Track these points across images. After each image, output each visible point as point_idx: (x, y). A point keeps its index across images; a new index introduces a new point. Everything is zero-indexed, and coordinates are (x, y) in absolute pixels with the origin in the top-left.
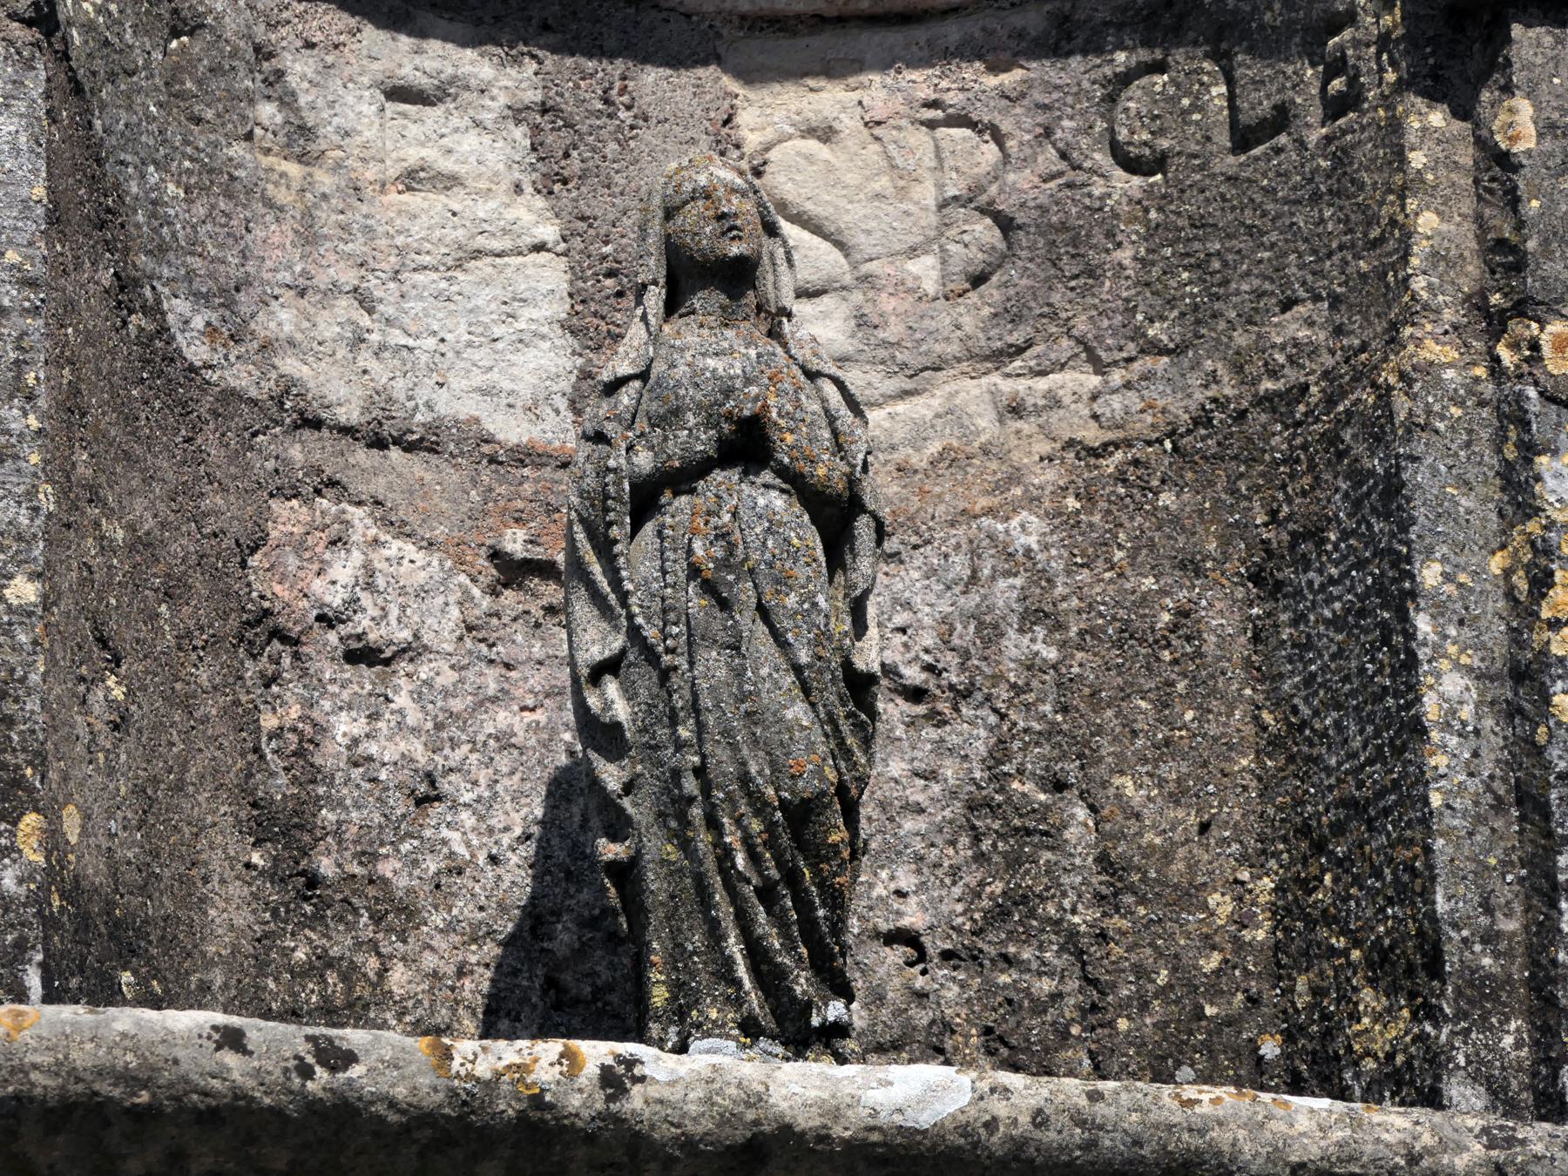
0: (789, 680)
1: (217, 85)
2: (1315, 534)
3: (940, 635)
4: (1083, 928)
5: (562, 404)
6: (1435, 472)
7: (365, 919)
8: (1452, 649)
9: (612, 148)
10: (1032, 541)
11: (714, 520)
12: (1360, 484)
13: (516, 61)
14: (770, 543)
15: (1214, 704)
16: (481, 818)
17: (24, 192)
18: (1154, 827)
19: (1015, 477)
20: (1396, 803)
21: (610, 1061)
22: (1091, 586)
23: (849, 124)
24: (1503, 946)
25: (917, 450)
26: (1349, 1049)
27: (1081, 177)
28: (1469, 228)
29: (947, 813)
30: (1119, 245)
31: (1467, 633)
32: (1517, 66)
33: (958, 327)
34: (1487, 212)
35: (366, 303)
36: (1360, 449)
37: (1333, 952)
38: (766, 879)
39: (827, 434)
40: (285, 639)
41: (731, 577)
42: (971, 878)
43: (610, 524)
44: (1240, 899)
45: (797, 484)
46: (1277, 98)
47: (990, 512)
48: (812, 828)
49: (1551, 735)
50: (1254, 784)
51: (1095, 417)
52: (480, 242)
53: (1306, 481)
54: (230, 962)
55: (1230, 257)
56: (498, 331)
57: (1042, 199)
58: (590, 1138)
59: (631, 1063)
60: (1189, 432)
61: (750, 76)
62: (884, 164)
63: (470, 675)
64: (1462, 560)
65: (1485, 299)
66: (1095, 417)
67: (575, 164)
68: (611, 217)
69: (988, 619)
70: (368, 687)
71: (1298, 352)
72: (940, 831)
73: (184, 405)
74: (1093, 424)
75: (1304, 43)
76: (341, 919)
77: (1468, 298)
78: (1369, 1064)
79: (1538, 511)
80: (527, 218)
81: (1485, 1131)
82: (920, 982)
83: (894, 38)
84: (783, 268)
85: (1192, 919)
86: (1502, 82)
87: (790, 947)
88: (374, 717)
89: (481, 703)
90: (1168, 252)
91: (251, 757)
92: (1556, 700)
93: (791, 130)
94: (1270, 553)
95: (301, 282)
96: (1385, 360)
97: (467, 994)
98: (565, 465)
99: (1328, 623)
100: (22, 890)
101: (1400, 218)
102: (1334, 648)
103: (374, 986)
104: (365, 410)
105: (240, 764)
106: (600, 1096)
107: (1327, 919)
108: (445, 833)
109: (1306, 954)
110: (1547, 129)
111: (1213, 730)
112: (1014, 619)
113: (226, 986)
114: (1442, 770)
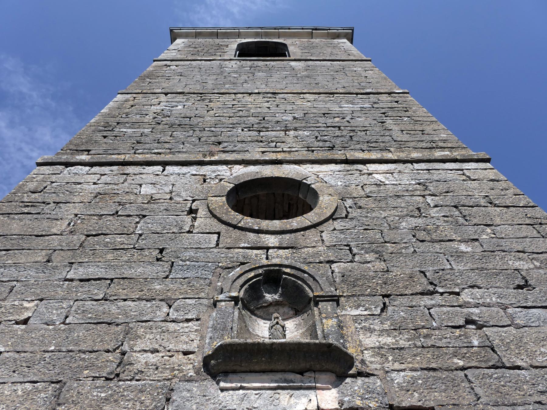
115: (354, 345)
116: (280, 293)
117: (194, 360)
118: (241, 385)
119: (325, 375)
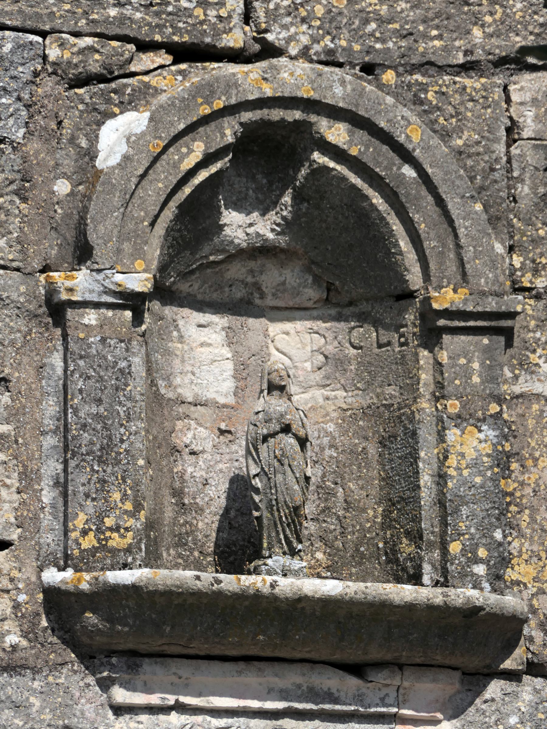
0: (295, 480)
1: (167, 331)
2: (395, 437)
5: (232, 394)
6: (424, 431)
9: (243, 336)
10: (332, 430)
13: (223, 317)
19: (327, 414)
23: (292, 332)
27: (343, 349)
28: (432, 377)
31: (430, 466)
35: (193, 374)
37: (396, 528)
39: (300, 423)
42: (317, 502)
45: (296, 437)
47: (322, 422)
52: (216, 358)
53: (393, 425)
54: (168, 525)
56: (219, 378)
58: (267, 598)
61: (272, 320)
63: (214, 457)
67: (235, 340)
71: (392, 397)
78: (404, 554)
79: (445, 442)
80: (225, 352)
81: (442, 593)
83: (302, 313)
84: (291, 385)
87: (292, 535)
88: (196, 467)
94: (383, 438)
108: (209, 492)
111: (370, 475)
112: (327, 447)
115: (535, 548)
116: (284, 218)
117: (12, 580)
118: (177, 701)
119: (434, 681)
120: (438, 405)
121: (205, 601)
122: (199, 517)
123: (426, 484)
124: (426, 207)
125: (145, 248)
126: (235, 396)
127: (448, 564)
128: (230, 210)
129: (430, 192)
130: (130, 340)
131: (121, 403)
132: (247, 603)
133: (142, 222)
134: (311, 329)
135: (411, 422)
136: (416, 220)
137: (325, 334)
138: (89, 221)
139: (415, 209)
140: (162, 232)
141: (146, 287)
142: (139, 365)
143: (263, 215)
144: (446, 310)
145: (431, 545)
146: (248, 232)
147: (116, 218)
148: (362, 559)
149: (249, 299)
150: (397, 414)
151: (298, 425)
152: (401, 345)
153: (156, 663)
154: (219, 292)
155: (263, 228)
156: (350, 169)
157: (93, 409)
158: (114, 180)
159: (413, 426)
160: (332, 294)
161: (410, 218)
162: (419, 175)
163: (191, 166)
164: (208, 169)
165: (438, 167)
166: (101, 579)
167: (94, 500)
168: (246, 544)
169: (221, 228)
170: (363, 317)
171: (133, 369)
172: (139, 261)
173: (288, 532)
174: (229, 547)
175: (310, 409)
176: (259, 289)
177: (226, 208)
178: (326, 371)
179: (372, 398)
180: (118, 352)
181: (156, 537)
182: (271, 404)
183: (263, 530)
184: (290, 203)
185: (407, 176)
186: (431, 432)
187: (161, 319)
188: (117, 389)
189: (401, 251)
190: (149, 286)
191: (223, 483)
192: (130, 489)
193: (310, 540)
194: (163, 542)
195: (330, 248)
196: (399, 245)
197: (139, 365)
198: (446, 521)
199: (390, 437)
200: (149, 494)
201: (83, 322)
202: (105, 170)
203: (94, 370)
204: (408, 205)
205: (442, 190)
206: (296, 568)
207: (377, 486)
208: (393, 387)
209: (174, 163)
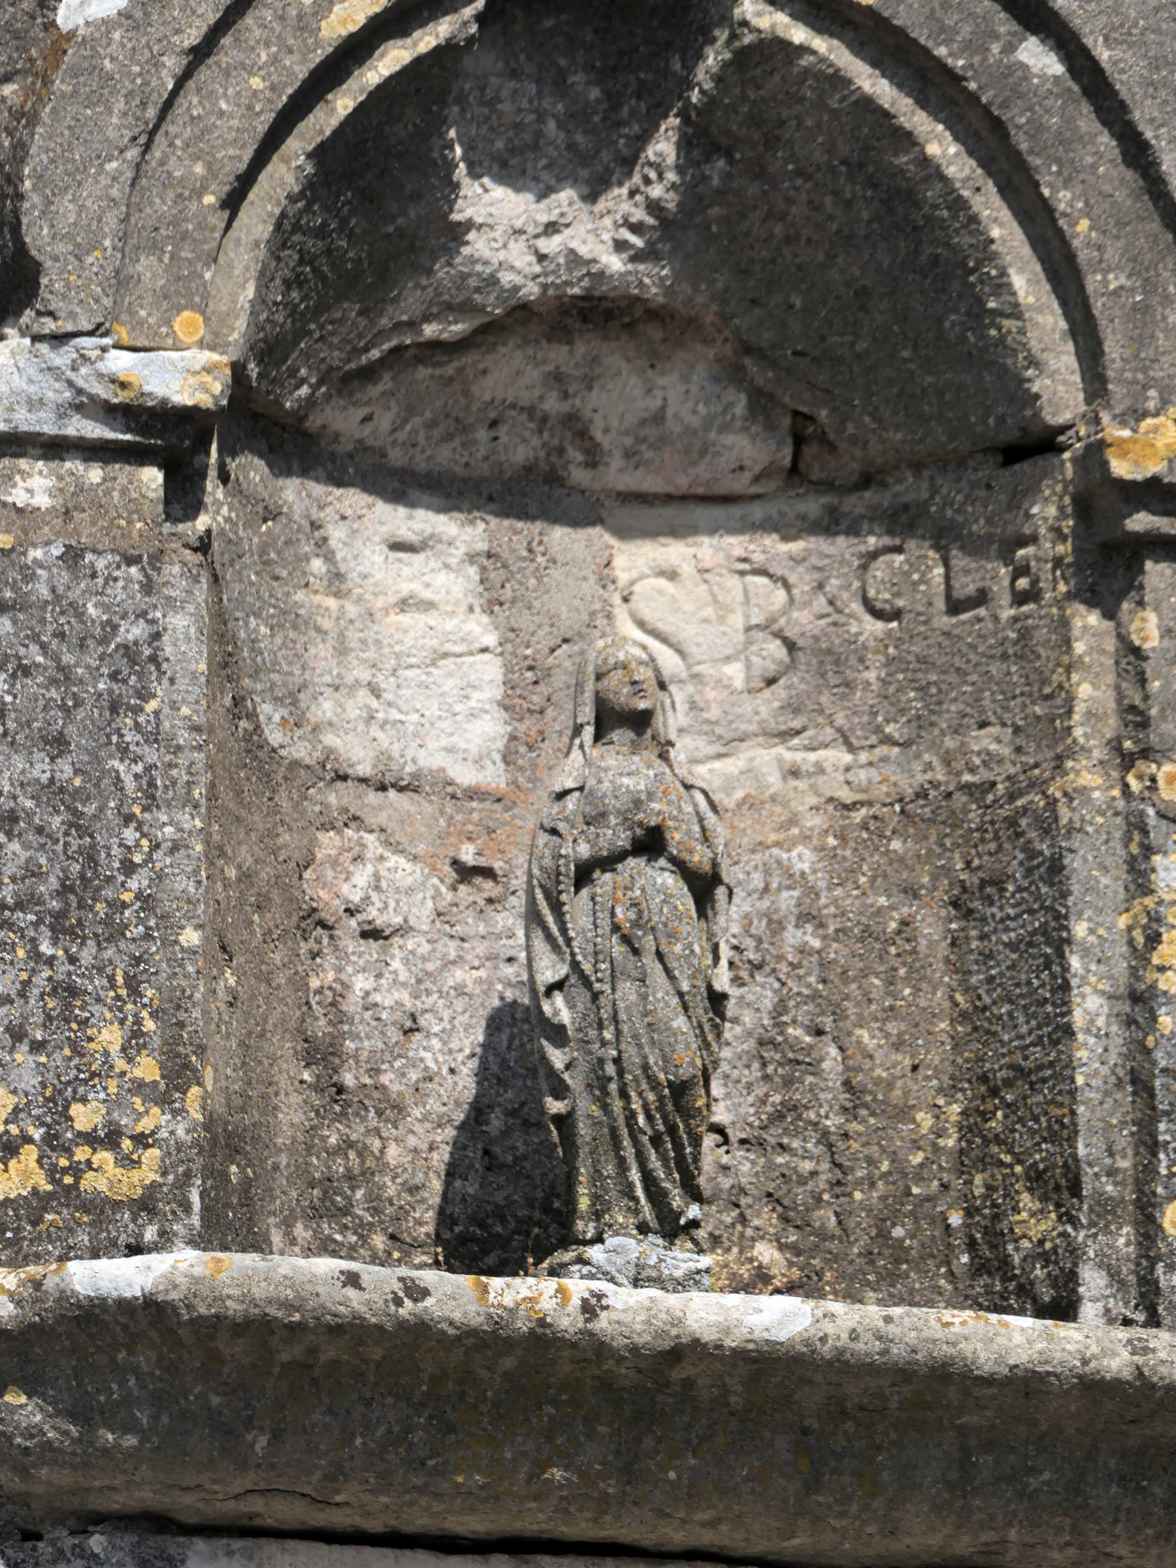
1: (289, 553)
2: (999, 883)
3: (743, 927)
4: (833, 1129)
5: (497, 757)
6: (1085, 861)
7: (372, 1114)
8: (1093, 979)
9: (532, 582)
10: (806, 867)
11: (629, 893)
12: (1032, 858)
13: (472, 522)
14: (665, 910)
15: (924, 985)
16: (445, 1043)
17: (193, 667)
18: (881, 1065)
19: (793, 821)
20: (1051, 1077)
21: (587, 1295)
22: (843, 899)
23: (687, 569)
24: (1120, 1178)
25: (728, 795)
26: (1012, 1230)
27: (842, 619)
28: (1111, 695)
29: (745, 1046)
30: (867, 668)
31: (1103, 968)
32: (1148, 590)
33: (757, 713)
34: (1124, 685)
35: (376, 692)
36: (1033, 834)
37: (1001, 1164)
38: (656, 1131)
39: (697, 828)
40: (322, 924)
41: (640, 933)
42: (760, 1091)
43: (560, 892)
44: (938, 1117)
46: (980, 584)
47: (777, 844)
48: (686, 1098)
49: (1157, 1043)
50: (949, 1040)
51: (848, 783)
52: (448, 647)
53: (993, 846)
54: (290, 1149)
55: (944, 687)
56: (458, 708)
57: (816, 632)
58: (573, 1345)
59: (600, 1296)
60: (912, 801)
61: (624, 533)
62: (709, 598)
63: (439, 946)
64: (1100, 919)
65: (1120, 743)
66: (848, 783)
67: (507, 593)
68: (531, 629)
69: (775, 917)
70: (375, 956)
71: (989, 759)
72: (740, 1058)
73: (268, 776)
74: (846, 787)
75: (1000, 550)
76: (358, 1114)
77: (1109, 742)
79: (1152, 892)
81: (1130, 1342)
82: (725, 1159)
83: (718, 512)
84: (670, 713)
85: (906, 1128)
86: (1137, 598)
87: (669, 1173)
88: (379, 976)
89: (445, 965)
90: (901, 676)
91: (304, 1009)
92: (1161, 1019)
93: (648, 572)
94: (965, 890)
95: (337, 681)
96: (1053, 779)
97: (435, 1163)
98: (499, 800)
99: (1006, 945)
100: (189, 1138)
101: (1066, 685)
102: (1009, 963)
103: (377, 1159)
104: (375, 766)
105: (298, 1013)
106: (581, 1319)
107: (998, 1140)
108: (422, 1053)
109: (982, 1160)
110: (1167, 632)
111: (923, 1003)
112: (793, 919)
113: (288, 1165)
114: (1084, 1061)
116: (653, 207)
120: (1131, 779)
121: (377, 1354)
122: (388, 1131)
123: (1092, 1021)
124: (1094, 167)
125: (208, 275)
126: (507, 763)
127: (1160, 1268)
128: (486, 180)
129: (1105, 123)
130: (157, 558)
131: (126, 750)
132: (508, 1363)
133: (199, 193)
134: (745, 560)
135: (1047, 831)
136: (1062, 207)
137: (787, 574)
138: (28, 184)
139: (1059, 173)
140: (264, 230)
141: (207, 391)
142: (188, 639)
143: (591, 197)
144: (1154, 482)
145: (1106, 1210)
146: (544, 251)
147: (114, 179)
148: (897, 1261)
149: (553, 469)
150: (1003, 813)
151: (689, 832)
152: (1020, 598)
153: (230, 1554)
154: (457, 442)
155: (591, 238)
156: (858, 49)
157: (39, 766)
158: (107, 63)
159: (1051, 846)
160: (810, 451)
161: (1044, 201)
162: (1071, 69)
163: (353, 28)
164: (409, 41)
165: (1131, 45)
166: (50, 1284)
167: (37, 1047)
168: (537, 1215)
169: (457, 233)
170: (904, 518)
171: (169, 650)
172: (186, 314)
173: (654, 1161)
174: (481, 1225)
175: (739, 805)
176: (583, 434)
177: (474, 174)
178: (789, 687)
179: (929, 767)
180: (117, 591)
181: (247, 1184)
182: (606, 770)
183: (575, 1157)
184: (671, 158)
185: (1035, 70)
186: (1109, 861)
187: (271, 514)
188: (114, 708)
189: (1017, 305)
190: (217, 388)
191: (467, 1027)
192: (154, 1015)
193: (737, 1206)
194: (273, 1199)
195: (798, 303)
196: (1009, 285)
197: (188, 639)
198: (1153, 1135)
199: (983, 883)
200: (223, 1046)
201: (10, 499)
202: (81, 32)
203: (44, 647)
204: (1035, 161)
205: (1144, 114)
206: (678, 1274)
207: (944, 1037)
208: (994, 730)
209: (300, 17)
